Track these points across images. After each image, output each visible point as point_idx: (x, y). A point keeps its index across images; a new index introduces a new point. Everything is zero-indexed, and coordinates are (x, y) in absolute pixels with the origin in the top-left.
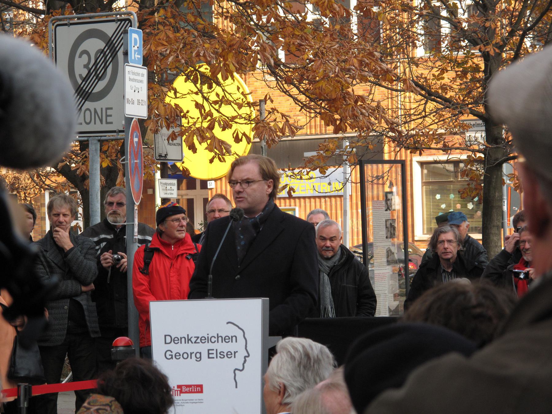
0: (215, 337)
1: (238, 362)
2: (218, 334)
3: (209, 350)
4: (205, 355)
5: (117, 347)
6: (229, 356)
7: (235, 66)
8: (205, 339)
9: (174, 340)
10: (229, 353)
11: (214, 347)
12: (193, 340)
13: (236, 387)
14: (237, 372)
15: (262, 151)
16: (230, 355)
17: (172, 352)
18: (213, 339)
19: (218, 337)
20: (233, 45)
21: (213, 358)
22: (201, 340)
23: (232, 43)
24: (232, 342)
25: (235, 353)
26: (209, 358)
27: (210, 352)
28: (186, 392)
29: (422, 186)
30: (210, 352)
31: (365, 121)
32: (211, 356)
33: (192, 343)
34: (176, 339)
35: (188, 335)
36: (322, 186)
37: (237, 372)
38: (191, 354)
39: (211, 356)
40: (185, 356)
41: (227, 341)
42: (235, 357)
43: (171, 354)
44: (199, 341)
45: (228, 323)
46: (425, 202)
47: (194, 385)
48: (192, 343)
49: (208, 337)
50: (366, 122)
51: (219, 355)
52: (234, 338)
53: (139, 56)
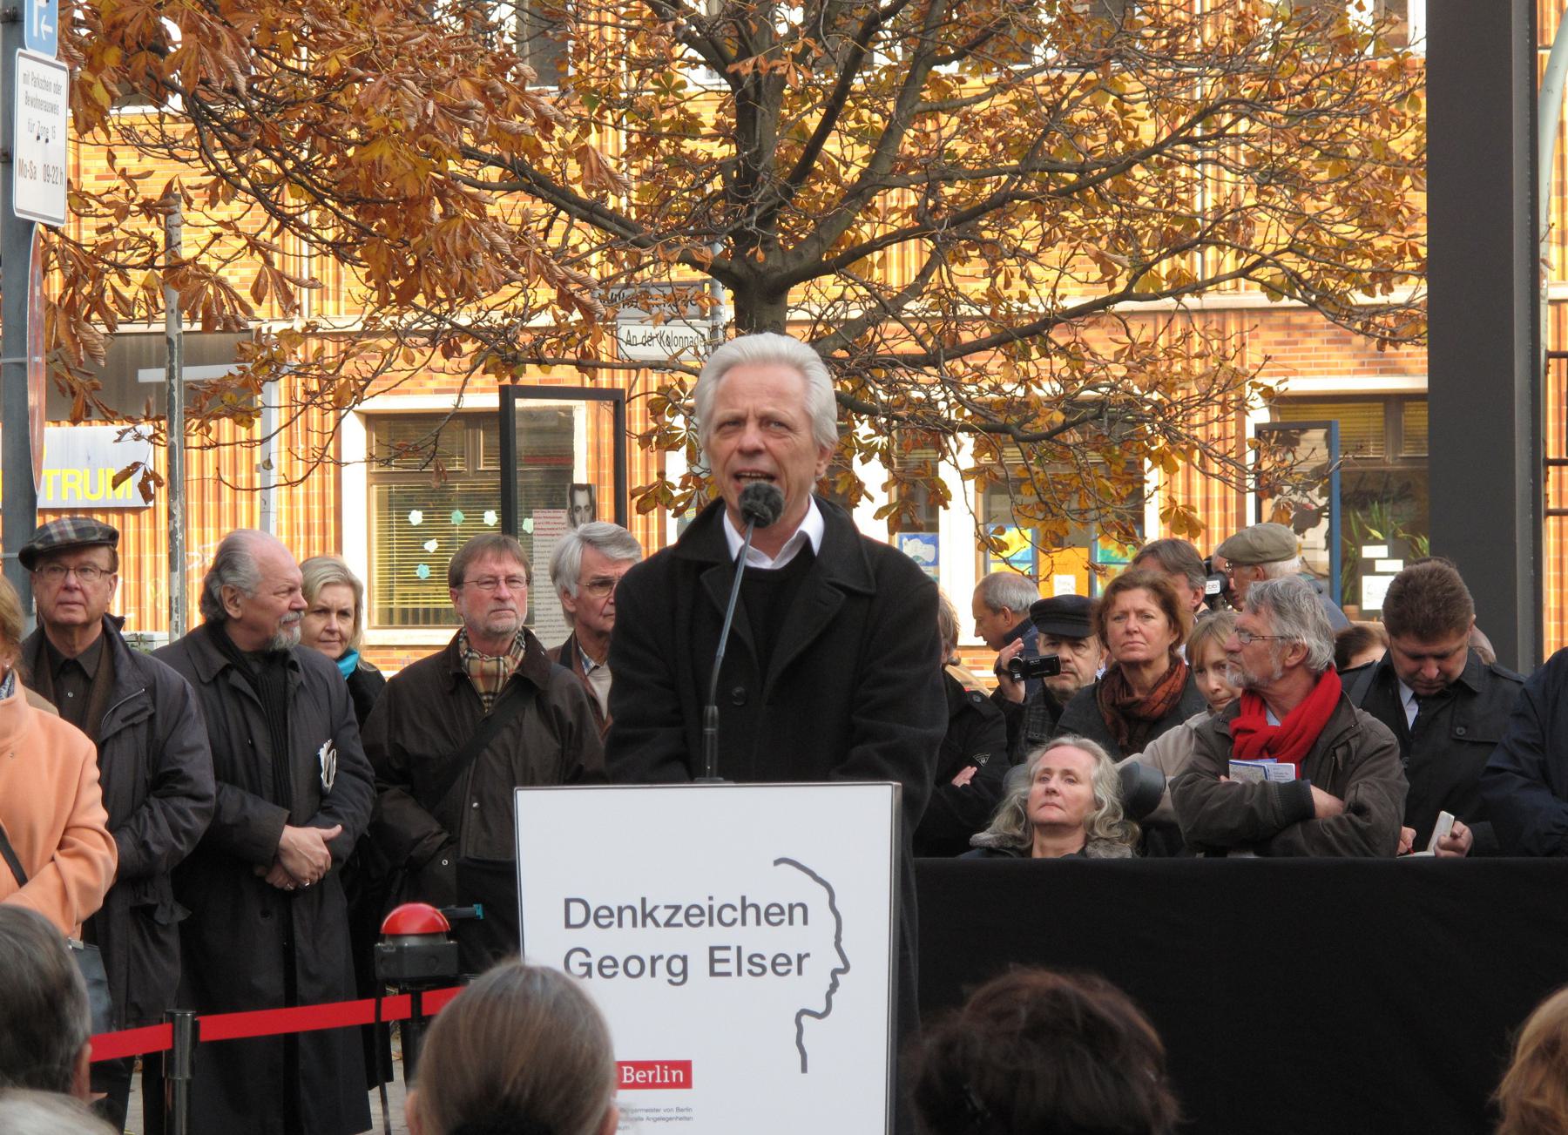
0: (734, 909)
1: (808, 989)
2: (743, 899)
3: (712, 949)
4: (698, 965)
5: (397, 936)
7: (109, 92)
8: (702, 914)
9: (596, 917)
10: (781, 960)
11: (732, 935)
12: (662, 915)
13: (804, 1069)
14: (805, 1019)
15: (172, 354)
16: (782, 964)
17: (588, 954)
18: (728, 915)
19: (744, 908)
20: (123, 23)
21: (728, 974)
22: (687, 915)
23: (120, 17)
24: (791, 922)
25: (800, 958)
26: (713, 973)
27: (718, 955)
28: (635, 1085)
29: (369, 485)
30: (718, 955)
31: (491, 269)
32: (719, 967)
33: (657, 924)
34: (604, 912)
35: (644, 900)
36: (65, 479)
37: (805, 1019)
38: (654, 960)
39: (719, 967)
40: (634, 967)
41: (774, 919)
42: (800, 972)
43: (586, 960)
44: (680, 918)
45: (777, 862)
46: (375, 533)
47: (662, 1063)
48: (657, 924)
49: (711, 908)
50: (493, 273)
51: (746, 966)
52: (798, 912)
53: (50, 29)
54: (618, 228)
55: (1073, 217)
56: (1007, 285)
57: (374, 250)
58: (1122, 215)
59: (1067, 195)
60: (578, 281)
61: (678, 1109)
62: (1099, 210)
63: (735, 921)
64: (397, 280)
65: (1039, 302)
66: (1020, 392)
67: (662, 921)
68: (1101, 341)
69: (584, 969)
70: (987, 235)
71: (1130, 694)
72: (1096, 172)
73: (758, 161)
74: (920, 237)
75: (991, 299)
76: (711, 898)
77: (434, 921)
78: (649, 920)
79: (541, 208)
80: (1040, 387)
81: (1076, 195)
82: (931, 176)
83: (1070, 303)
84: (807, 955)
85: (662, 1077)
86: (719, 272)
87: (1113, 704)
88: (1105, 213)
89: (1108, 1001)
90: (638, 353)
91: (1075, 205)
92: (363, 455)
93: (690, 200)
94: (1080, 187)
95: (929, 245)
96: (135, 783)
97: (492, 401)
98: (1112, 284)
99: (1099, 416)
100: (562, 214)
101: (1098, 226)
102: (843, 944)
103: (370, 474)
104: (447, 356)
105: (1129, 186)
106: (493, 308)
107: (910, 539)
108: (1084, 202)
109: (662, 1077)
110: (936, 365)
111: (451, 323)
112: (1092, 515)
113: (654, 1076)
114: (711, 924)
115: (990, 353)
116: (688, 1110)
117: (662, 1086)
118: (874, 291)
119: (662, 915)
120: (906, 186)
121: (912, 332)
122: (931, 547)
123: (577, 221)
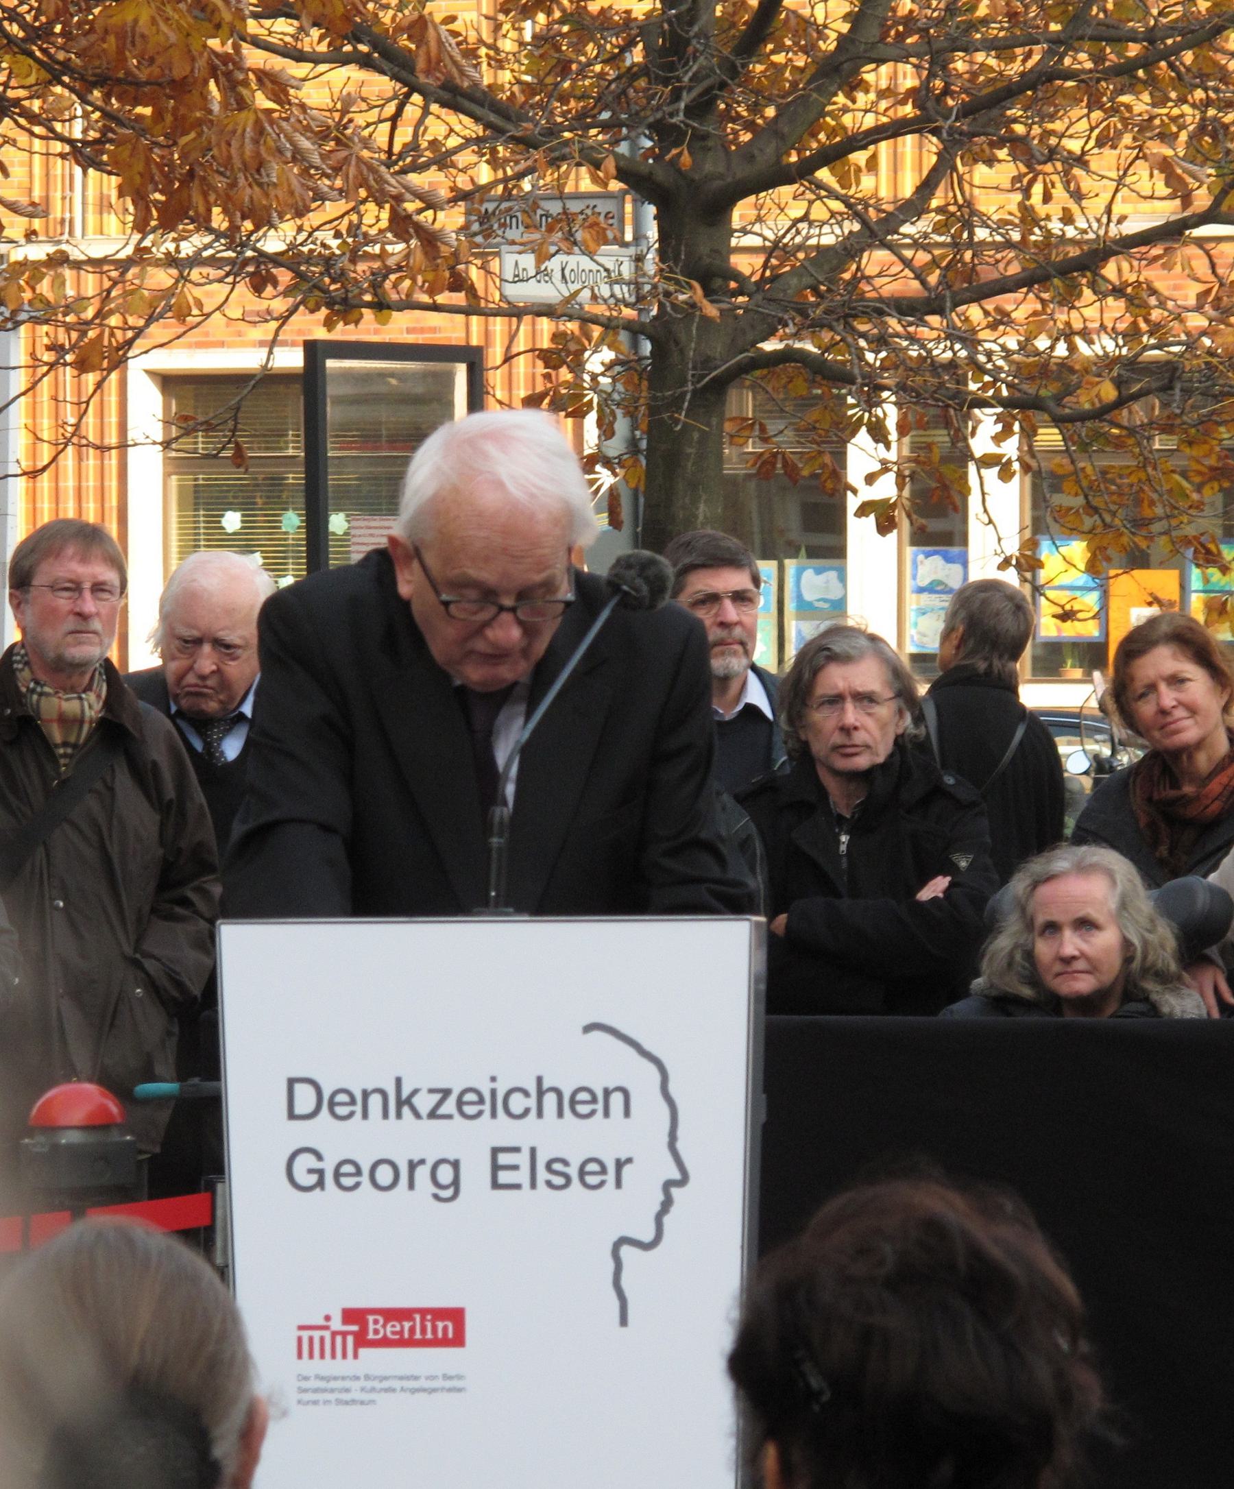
0: (526, 1094)
1: (631, 1208)
2: (539, 1080)
3: (495, 1151)
4: (476, 1174)
8: (481, 1101)
11: (521, 1130)
12: (424, 1103)
13: (624, 1321)
14: (626, 1251)
16: (597, 1173)
17: (319, 1157)
19: (541, 1093)
21: (517, 1187)
22: (460, 1103)
24: (607, 1114)
25: (620, 1165)
26: (496, 1185)
27: (503, 1159)
28: (385, 1342)
29: (167, 475)
30: (503, 1159)
32: (504, 1177)
33: (417, 1115)
35: (398, 1081)
37: (626, 1251)
38: (412, 1166)
39: (504, 1177)
42: (619, 1184)
43: (317, 1165)
44: (449, 1106)
45: (588, 1028)
47: (423, 1312)
48: (417, 1115)
49: (493, 1093)
51: (542, 1175)
52: (617, 1100)
54: (493, 118)
55: (1140, 103)
56: (1047, 198)
57: (126, 154)
58: (1208, 103)
59: (1125, 74)
60: (418, 195)
61: (446, 1377)
62: (1173, 95)
64: (165, 197)
65: (1085, 225)
66: (1061, 350)
67: (424, 1109)
68: (1179, 283)
69: (314, 1178)
70: (1019, 129)
71: (1176, 785)
72: (1170, 41)
73: (691, 24)
74: (918, 131)
75: (1023, 220)
77: (104, 1110)
78: (406, 1110)
79: (381, 85)
80: (1090, 342)
81: (1141, 73)
82: (936, 46)
83: (1131, 227)
84: (629, 1160)
85: (424, 1331)
86: (638, 181)
87: (1150, 800)
88: (1182, 100)
89: (1016, 1241)
90: (522, 293)
91: (1140, 87)
92: (158, 435)
93: (601, 75)
94: (1146, 62)
95: (933, 144)
96: (857, 746)
97: (291, 359)
98: (1187, 200)
99: (1167, 388)
100: (416, 98)
101: (1174, 119)
102: (680, 1145)
103: (167, 460)
104: (258, 289)
105: (1216, 64)
106: (321, 228)
107: (928, 555)
108: (1152, 83)
109: (424, 1331)
110: (940, 312)
111: (255, 249)
112: (1156, 527)
113: (412, 1330)
114: (494, 1114)
115: (1019, 295)
116: (460, 1377)
117: (424, 1343)
118: (854, 209)
119: (424, 1103)
120: (903, 58)
121: (907, 263)
122: (957, 568)
123: (434, 107)
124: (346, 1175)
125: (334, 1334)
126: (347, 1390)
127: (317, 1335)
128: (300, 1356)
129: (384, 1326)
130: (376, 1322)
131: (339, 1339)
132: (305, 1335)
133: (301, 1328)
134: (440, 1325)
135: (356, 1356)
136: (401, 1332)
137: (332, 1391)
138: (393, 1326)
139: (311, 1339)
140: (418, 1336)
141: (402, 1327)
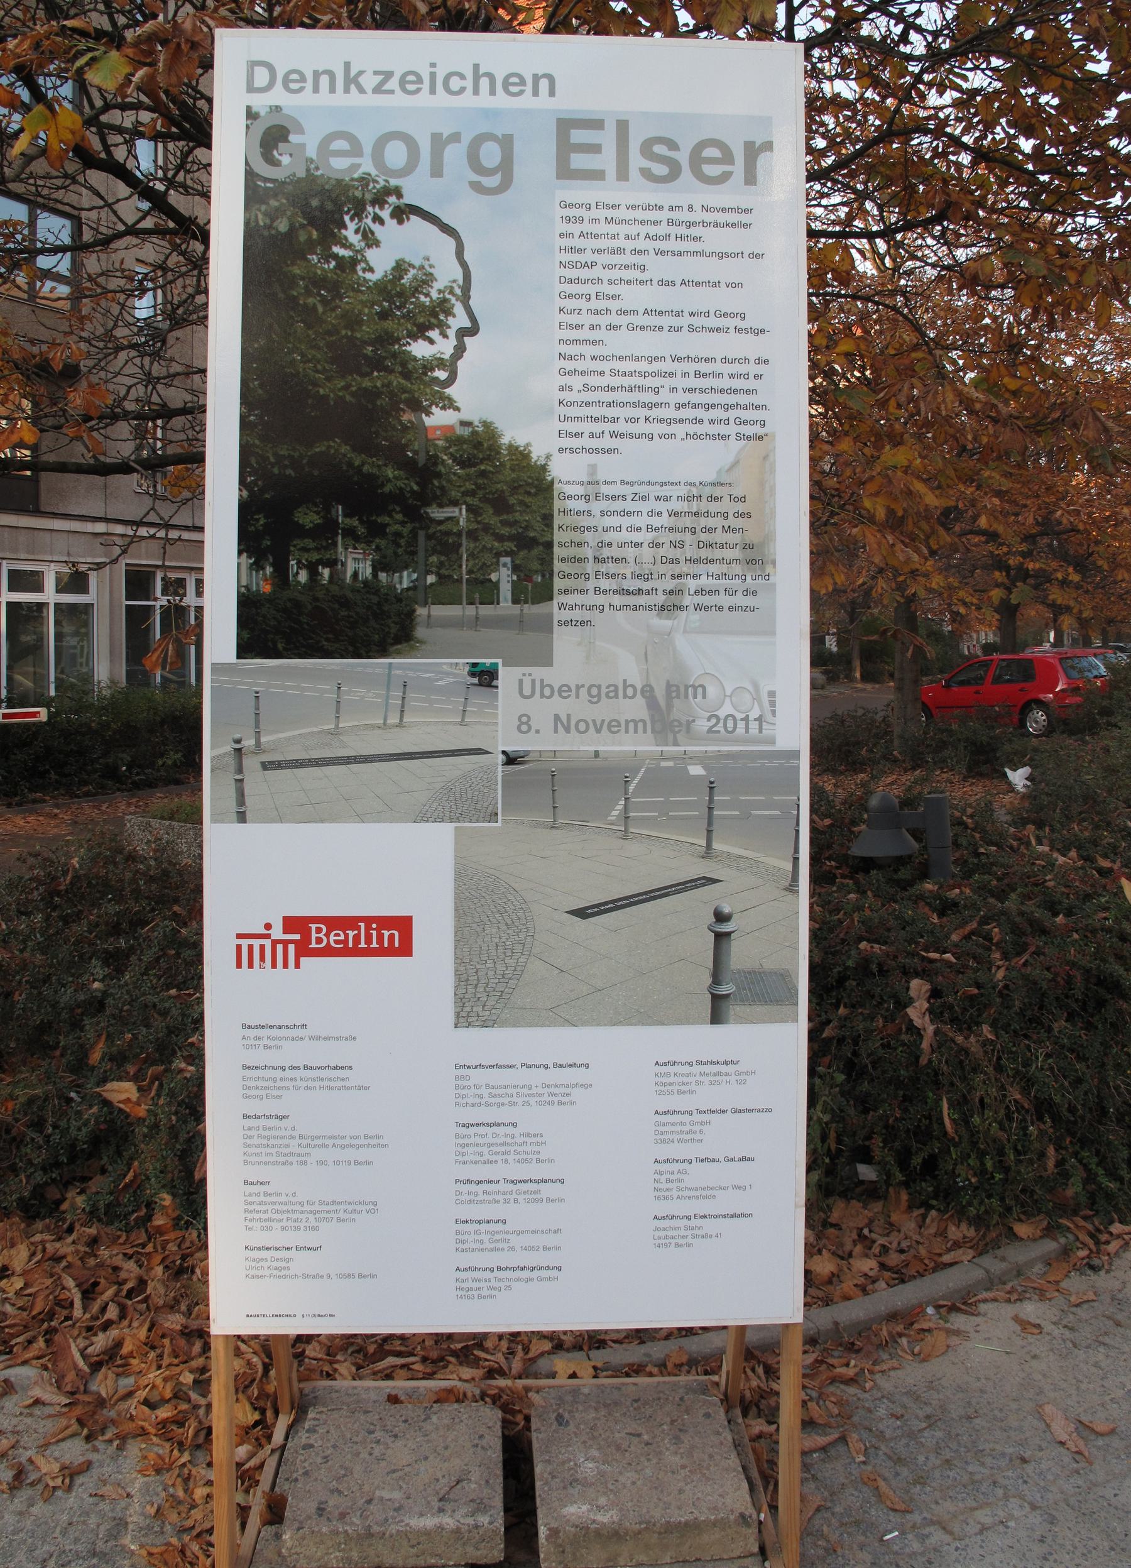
0: (462, 77)
2: (476, 67)
6: (711, 170)
12: (369, 81)
21: (598, 175)
22: (403, 82)
27: (578, 136)
30: (578, 136)
32: (578, 161)
33: (362, 90)
35: (347, 65)
39: (578, 161)
47: (368, 920)
48: (362, 90)
49: (433, 76)
51: (636, 160)
52: (544, 84)
63: (463, 90)
76: (433, 65)
78: (353, 87)
85: (369, 940)
109: (369, 940)
113: (357, 939)
124: (250, 1097)
125: (275, 943)
126: (286, 1146)
127: (256, 943)
128: (239, 966)
129: (327, 935)
130: (319, 930)
131: (280, 947)
132: (245, 943)
133: (239, 936)
134: (386, 934)
135: (297, 966)
136: (346, 941)
137: (273, 1146)
138: (337, 935)
139: (251, 947)
140: (363, 945)
141: (346, 936)
